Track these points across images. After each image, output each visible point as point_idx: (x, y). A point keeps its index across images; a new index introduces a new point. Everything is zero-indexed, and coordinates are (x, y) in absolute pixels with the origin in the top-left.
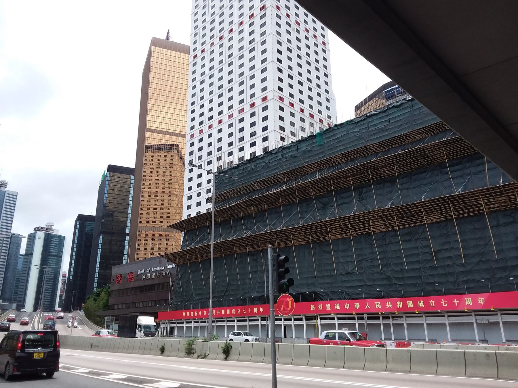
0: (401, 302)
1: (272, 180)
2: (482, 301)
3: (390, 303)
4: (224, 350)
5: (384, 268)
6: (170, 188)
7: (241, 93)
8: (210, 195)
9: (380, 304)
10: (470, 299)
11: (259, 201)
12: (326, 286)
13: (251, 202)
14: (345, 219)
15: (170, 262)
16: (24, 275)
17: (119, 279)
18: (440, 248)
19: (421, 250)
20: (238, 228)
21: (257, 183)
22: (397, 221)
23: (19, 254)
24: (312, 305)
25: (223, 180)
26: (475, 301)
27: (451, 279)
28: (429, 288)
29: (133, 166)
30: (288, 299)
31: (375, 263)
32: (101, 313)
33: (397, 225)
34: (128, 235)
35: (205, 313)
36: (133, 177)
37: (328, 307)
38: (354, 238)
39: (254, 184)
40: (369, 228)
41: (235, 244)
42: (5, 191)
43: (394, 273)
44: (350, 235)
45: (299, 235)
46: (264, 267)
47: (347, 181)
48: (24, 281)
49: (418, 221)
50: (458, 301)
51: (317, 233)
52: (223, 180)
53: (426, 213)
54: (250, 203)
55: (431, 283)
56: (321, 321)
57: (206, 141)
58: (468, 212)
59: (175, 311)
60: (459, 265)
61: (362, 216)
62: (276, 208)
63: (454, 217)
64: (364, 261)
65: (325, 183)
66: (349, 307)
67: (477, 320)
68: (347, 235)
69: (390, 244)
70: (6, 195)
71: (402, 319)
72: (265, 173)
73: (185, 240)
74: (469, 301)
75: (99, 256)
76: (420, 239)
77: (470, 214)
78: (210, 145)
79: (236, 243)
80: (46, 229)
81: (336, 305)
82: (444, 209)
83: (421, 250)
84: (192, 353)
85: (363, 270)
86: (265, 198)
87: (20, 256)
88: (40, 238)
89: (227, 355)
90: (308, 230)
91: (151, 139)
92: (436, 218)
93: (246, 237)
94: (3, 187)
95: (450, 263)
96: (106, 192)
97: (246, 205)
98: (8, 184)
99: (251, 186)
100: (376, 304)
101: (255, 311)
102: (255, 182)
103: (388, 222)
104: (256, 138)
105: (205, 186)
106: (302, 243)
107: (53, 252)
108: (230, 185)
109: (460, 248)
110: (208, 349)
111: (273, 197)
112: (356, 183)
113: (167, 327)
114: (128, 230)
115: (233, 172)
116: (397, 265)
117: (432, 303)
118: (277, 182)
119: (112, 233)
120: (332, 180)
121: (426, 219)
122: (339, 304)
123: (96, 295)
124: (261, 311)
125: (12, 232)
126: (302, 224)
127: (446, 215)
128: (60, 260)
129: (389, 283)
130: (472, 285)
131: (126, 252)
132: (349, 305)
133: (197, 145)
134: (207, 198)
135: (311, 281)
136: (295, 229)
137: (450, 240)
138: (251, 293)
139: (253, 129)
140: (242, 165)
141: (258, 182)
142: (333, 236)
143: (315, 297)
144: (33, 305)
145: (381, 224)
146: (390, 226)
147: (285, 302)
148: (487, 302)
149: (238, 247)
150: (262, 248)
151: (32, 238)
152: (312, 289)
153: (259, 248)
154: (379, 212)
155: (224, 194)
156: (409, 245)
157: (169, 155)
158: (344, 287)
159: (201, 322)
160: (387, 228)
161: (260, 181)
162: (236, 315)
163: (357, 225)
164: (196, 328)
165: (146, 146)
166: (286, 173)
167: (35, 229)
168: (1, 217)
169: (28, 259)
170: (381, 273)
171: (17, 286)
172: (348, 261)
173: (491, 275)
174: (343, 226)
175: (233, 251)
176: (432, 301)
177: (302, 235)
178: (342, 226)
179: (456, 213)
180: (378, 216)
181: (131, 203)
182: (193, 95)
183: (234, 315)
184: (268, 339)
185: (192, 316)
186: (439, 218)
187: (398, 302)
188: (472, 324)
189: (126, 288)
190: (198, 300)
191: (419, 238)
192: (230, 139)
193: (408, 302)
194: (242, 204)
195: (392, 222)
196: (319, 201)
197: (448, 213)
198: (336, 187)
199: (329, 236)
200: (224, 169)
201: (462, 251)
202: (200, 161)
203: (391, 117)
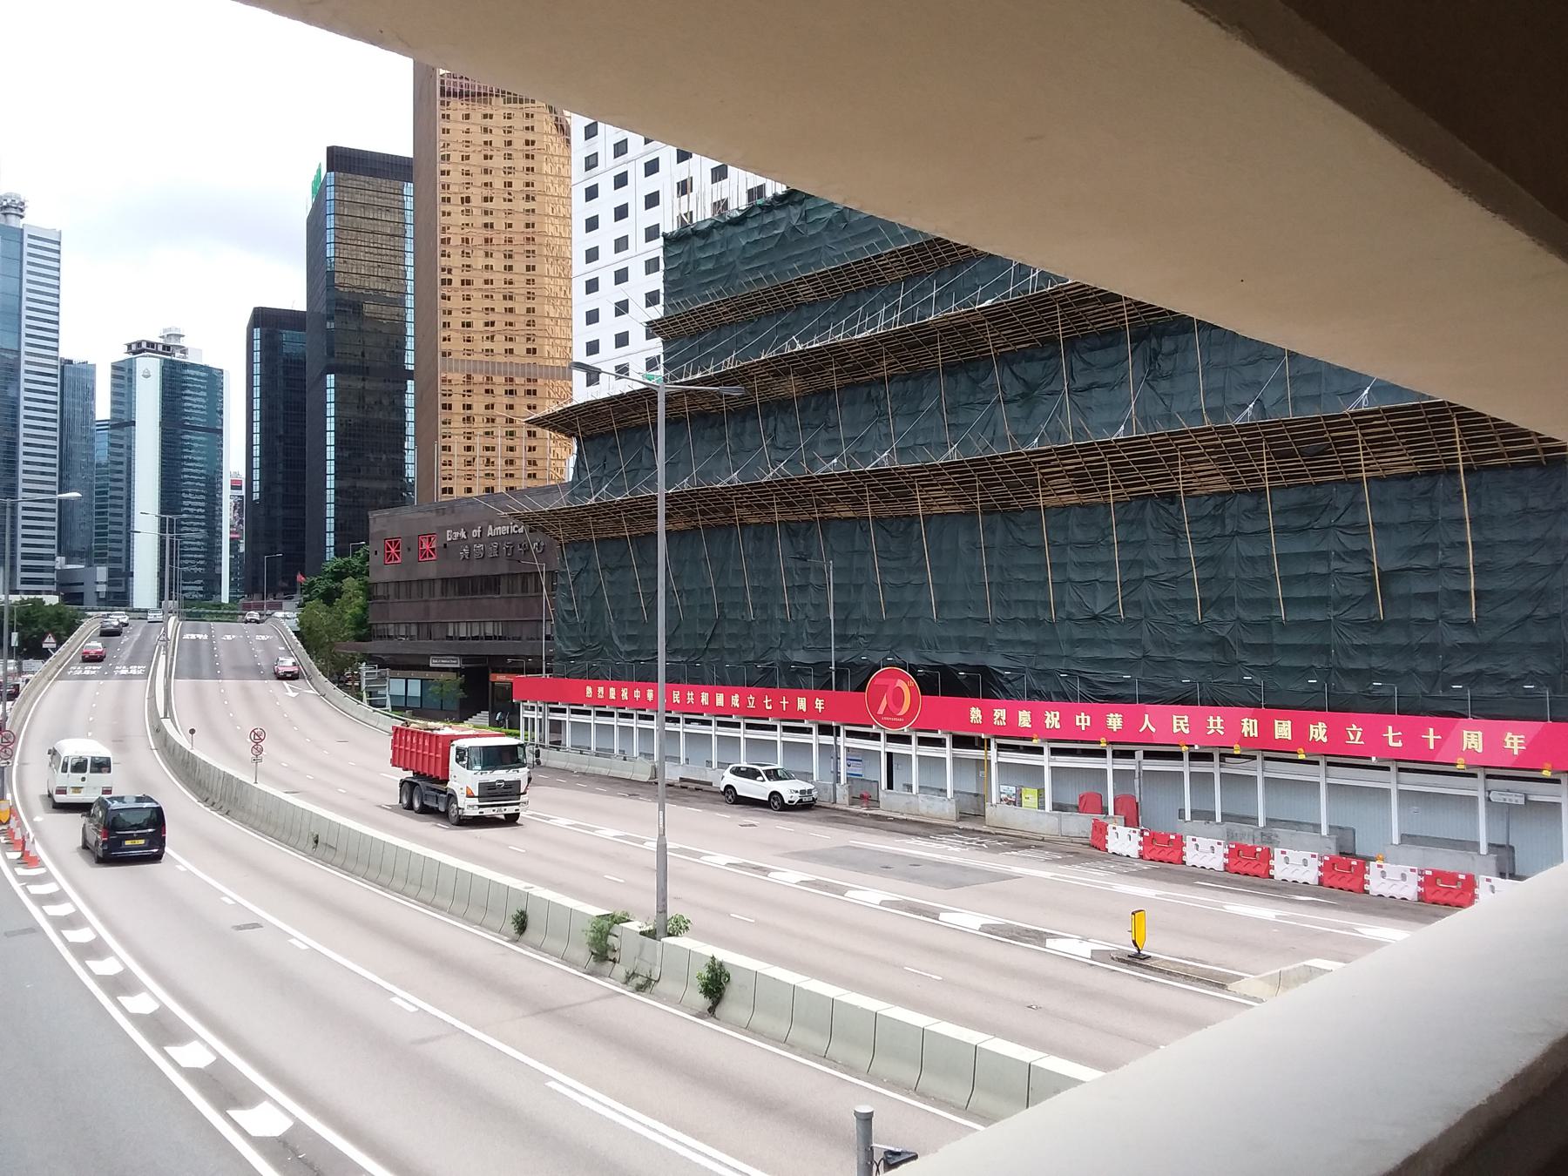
0: (1256, 721)
1: (857, 274)
2: (1516, 744)
3: (1219, 720)
4: (705, 986)
5: (1209, 611)
6: (531, 255)
8: (657, 312)
9: (1186, 721)
10: (1480, 733)
11: (815, 362)
12: (1020, 649)
13: (789, 363)
14: (1096, 449)
16: (119, 468)
17: (393, 550)
18: (1399, 565)
19: (1335, 565)
20: (748, 441)
21: (809, 282)
22: (1267, 464)
23: (94, 421)
24: (973, 708)
25: (697, 262)
26: (1493, 742)
27: (1425, 666)
28: (1351, 688)
29: (403, 146)
30: (901, 683)
31: (1184, 594)
32: (347, 648)
33: (1266, 476)
34: (410, 375)
36: (409, 188)
37: (1024, 719)
38: (1121, 505)
39: (798, 284)
40: (1172, 480)
41: (736, 499)
42: (21, 227)
43: (1241, 629)
44: (1109, 496)
45: (940, 487)
46: (829, 574)
47: (1110, 310)
48: (119, 502)
49: (1339, 468)
50: (1439, 737)
51: (1000, 484)
52: (697, 262)
53: (1370, 447)
54: (784, 364)
55: (1357, 671)
56: (1000, 753)
58: (1511, 454)
59: (562, 679)
60: (1456, 624)
61: (1152, 444)
62: (869, 384)
63: (1461, 463)
64: (1146, 585)
65: (1035, 314)
66: (1088, 724)
67: (1489, 792)
68: (1099, 497)
69: (1238, 534)
70: (27, 241)
72: (833, 244)
73: (581, 466)
74: (1473, 740)
75: (330, 439)
76: (1338, 527)
79: (740, 496)
80: (164, 349)
81: (1048, 714)
82: (1431, 440)
83: (1335, 565)
84: (610, 960)
85: (1141, 610)
86: (834, 353)
87: (98, 426)
88: (148, 377)
89: (715, 999)
90: (973, 476)
92: (1400, 462)
93: (771, 482)
94: (13, 217)
95: (1427, 613)
96: (330, 237)
97: (772, 371)
99: (787, 291)
100: (1175, 721)
101: (799, 707)
102: (801, 279)
103: (1238, 467)
105: (642, 314)
106: (949, 509)
108: (719, 280)
109: (1469, 568)
110: (658, 963)
111: (862, 351)
112: (1140, 318)
113: (540, 720)
115: (730, 235)
116: (1249, 603)
117: (1354, 733)
118: (873, 281)
119: (363, 371)
120: (1061, 307)
121: (1365, 465)
122: (1058, 713)
124: (817, 707)
125: (60, 356)
126: (953, 454)
127: (1438, 457)
129: (1221, 659)
130: (1490, 690)
131: (410, 429)
132: (1088, 718)
133: (609, 199)
134: (647, 323)
135: (971, 633)
136: (930, 471)
137: (1439, 541)
138: (789, 651)
140: (758, 211)
141: (810, 279)
142: (1053, 495)
144: (157, 571)
145: (1214, 472)
146: (1244, 477)
147: (890, 690)
148: (1532, 746)
149: (746, 506)
150: (821, 515)
151: (123, 375)
152: (977, 658)
153: (814, 516)
154: (1213, 434)
155: (703, 311)
156: (1299, 546)
158: (1076, 660)
159: (641, 717)
160: (1231, 484)
161: (818, 274)
162: (743, 711)
163: (1133, 470)
164: (627, 731)
166: (905, 252)
167: (129, 346)
169: (122, 438)
170: (1199, 627)
171: (103, 513)
172: (1097, 580)
173: (1557, 664)
174: (1087, 471)
175: (731, 517)
176: (1354, 728)
177: (951, 486)
178: (1083, 468)
179: (1470, 453)
180: (1205, 447)
183: (737, 711)
184: (837, 786)
185: (614, 698)
186: (1411, 465)
187: (1245, 720)
190: (629, 654)
191: (1337, 524)
193: (1276, 722)
194: (757, 367)
195: (1253, 466)
198: (1072, 328)
199: (1038, 496)
200: (698, 223)
201: (1468, 524)
202: (621, 159)
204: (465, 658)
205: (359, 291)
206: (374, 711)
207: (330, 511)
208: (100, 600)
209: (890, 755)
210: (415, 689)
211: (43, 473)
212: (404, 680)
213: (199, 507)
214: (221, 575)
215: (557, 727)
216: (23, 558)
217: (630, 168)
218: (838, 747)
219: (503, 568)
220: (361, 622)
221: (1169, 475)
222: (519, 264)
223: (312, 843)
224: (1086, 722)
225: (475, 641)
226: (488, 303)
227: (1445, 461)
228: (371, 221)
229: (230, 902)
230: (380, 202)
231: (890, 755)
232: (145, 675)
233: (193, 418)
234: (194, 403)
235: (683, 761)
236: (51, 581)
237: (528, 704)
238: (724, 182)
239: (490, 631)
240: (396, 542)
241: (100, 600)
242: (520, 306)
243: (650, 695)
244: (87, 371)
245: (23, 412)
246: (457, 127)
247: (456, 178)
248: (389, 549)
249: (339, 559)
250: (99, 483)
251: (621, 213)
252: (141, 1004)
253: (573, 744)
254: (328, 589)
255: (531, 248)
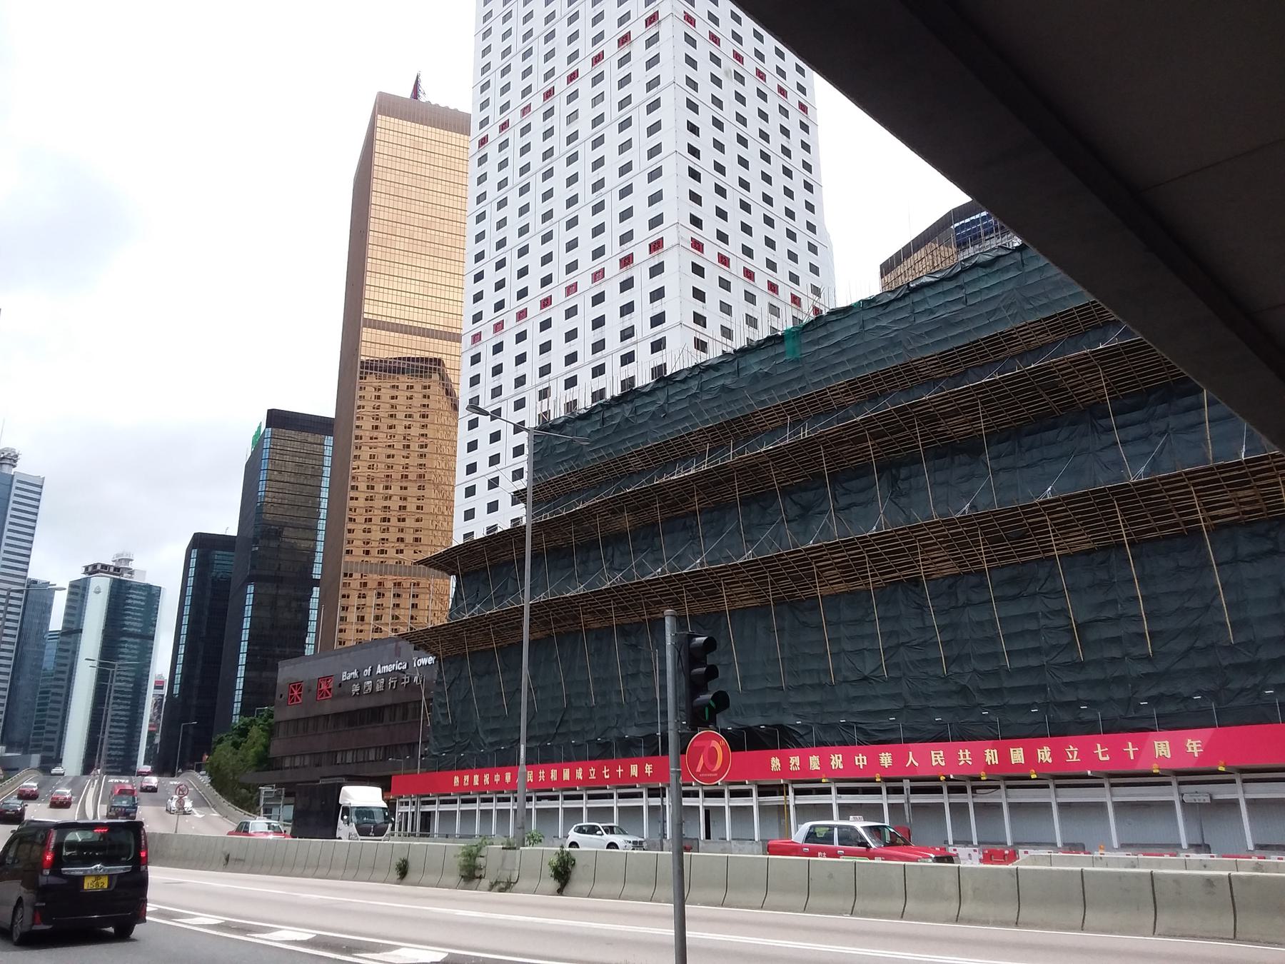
0: (995, 751)
1: (675, 448)
2: (1195, 748)
3: (967, 753)
4: (555, 869)
5: (952, 666)
6: (423, 467)
7: (598, 231)
8: (521, 484)
9: (942, 755)
10: (1167, 742)
11: (643, 500)
12: (808, 709)
13: (623, 502)
14: (856, 543)
15: (422, 652)
16: (60, 683)
17: (296, 693)
18: (1092, 616)
19: (1043, 622)
20: (591, 566)
21: (638, 455)
22: (984, 549)
23: (47, 631)
24: (773, 758)
25: (554, 447)
26: (1178, 748)
27: (1119, 693)
28: (1065, 716)
30: (715, 744)
31: (931, 654)
32: (250, 777)
33: (984, 559)
34: (317, 583)
36: (329, 440)
37: (814, 763)
38: (878, 590)
39: (630, 457)
40: (915, 567)
41: (582, 606)
42: (12, 474)
43: (977, 678)
44: (869, 583)
45: (741, 584)
46: (655, 663)
47: (860, 449)
48: (59, 698)
49: (1037, 548)
50: (1137, 749)
51: (786, 578)
52: (554, 447)
53: (1057, 529)
54: (620, 503)
56: (797, 796)
57: (512, 350)
58: (1162, 528)
59: (434, 773)
60: (1139, 659)
61: (897, 537)
62: (686, 516)
63: (1125, 539)
65: (805, 454)
66: (865, 763)
67: (1182, 795)
68: (862, 585)
69: (969, 605)
70: (15, 484)
71: (997, 792)
72: (656, 429)
73: (459, 596)
74: (1162, 748)
75: (245, 635)
76: (1042, 593)
77: (1166, 532)
78: (521, 359)
79: (585, 603)
80: (115, 570)
81: (833, 757)
82: (1101, 520)
83: (1043, 622)
84: (477, 878)
85: (900, 670)
86: (658, 492)
87: (50, 635)
88: (99, 592)
89: (563, 881)
90: (765, 573)
91: (375, 346)
92: (1081, 541)
93: (610, 589)
94: (8, 466)
95: (1115, 652)
96: (263, 476)
97: (610, 510)
98: (19, 456)
99: (622, 463)
100: (933, 755)
101: (632, 774)
102: (632, 453)
103: (963, 553)
104: (636, 343)
106: (749, 603)
107: (132, 626)
108: (571, 459)
109: (1142, 616)
110: (517, 868)
111: (678, 489)
112: (882, 455)
113: (413, 813)
114: (317, 571)
115: (579, 426)
116: (984, 657)
117: (1072, 752)
118: (686, 453)
119: (277, 580)
120: (824, 448)
121: (1056, 545)
122: (840, 756)
123: (238, 734)
124: (646, 772)
125: (29, 576)
126: (748, 555)
127: (1107, 534)
129: (964, 703)
130: (1171, 708)
131: (312, 627)
132: (865, 758)
134: (514, 493)
135: (770, 699)
136: (732, 570)
137: (1117, 597)
138: (623, 728)
139: (627, 321)
140: (600, 409)
141: (639, 453)
142: (826, 585)
143: (781, 738)
144: (82, 758)
145: (946, 558)
146: (968, 561)
147: (706, 751)
148: (1208, 749)
149: (590, 612)
150: (649, 617)
151: (78, 592)
152: (775, 718)
153: (643, 617)
154: (941, 526)
155: (557, 482)
156: (1014, 610)
157: (418, 384)
158: (853, 714)
159: (499, 800)
160: (959, 567)
161: (645, 449)
162: (586, 783)
163: (885, 560)
164: (486, 814)
165: (362, 362)
166: (710, 430)
167: (87, 568)
169: (68, 643)
170: (945, 679)
171: (43, 710)
173: (1218, 683)
174: (851, 563)
175: (577, 624)
176: (1072, 748)
177: (749, 583)
178: (847, 561)
179: (1132, 529)
180: (937, 537)
181: (324, 504)
182: (480, 237)
183: (580, 782)
184: (664, 841)
185: (478, 784)
186: (1089, 542)
187: (987, 751)
188: (1171, 804)
189: (312, 714)
190: (492, 744)
191: (1040, 591)
192: (570, 346)
193: (1011, 750)
194: (599, 506)
195: (973, 551)
197: (1111, 529)
198: (833, 465)
199: (815, 587)
200: (555, 420)
201: (1145, 623)
202: (496, 399)
203: (970, 291)
215: (427, 817)
221: (912, 562)
224: (859, 759)
240: (299, 686)
243: (508, 777)
246: (370, 393)
247: (363, 465)
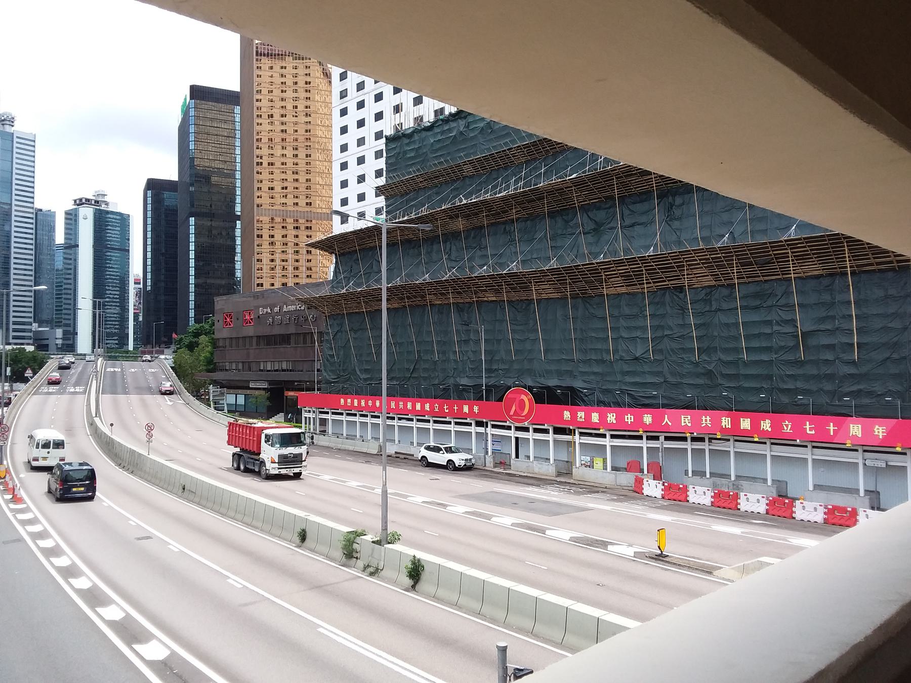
0: (729, 419)
1: (498, 159)
2: (881, 432)
3: (708, 418)
4: (410, 573)
5: (703, 355)
6: (308, 148)
8: (382, 181)
9: (689, 419)
10: (860, 426)
11: (473, 210)
12: (593, 377)
13: (458, 211)
14: (637, 261)
16: (69, 272)
17: (228, 320)
18: (813, 328)
19: (776, 328)
20: (435, 256)
21: (470, 164)
22: (736, 270)
23: (54, 245)
24: (565, 411)
25: (405, 152)
26: (867, 431)
27: (828, 387)
28: (785, 400)
29: (234, 85)
30: (523, 397)
31: (688, 345)
32: (202, 377)
33: (736, 277)
34: (238, 218)
35: (378, 404)
36: (237, 109)
37: (595, 417)
38: (651, 294)
39: (464, 165)
40: (681, 279)
41: (428, 290)
42: (12, 132)
43: (721, 365)
44: (644, 288)
45: (546, 283)
46: (482, 334)
47: (645, 180)
48: (69, 292)
49: (778, 272)
50: (836, 428)
51: (581, 281)
52: (405, 152)
53: (796, 259)
54: (456, 212)
56: (581, 437)
58: (878, 264)
59: (327, 394)
60: (846, 363)
61: (669, 258)
62: (505, 223)
63: (849, 269)
65: (601, 182)
66: (632, 420)
67: (865, 460)
68: (639, 289)
69: (719, 310)
70: (15, 140)
72: (484, 142)
73: (338, 271)
74: (856, 430)
75: (192, 255)
76: (777, 306)
79: (430, 288)
80: (95, 202)
81: (609, 415)
82: (831, 255)
83: (776, 328)
84: (355, 558)
85: (663, 354)
86: (485, 205)
87: (57, 247)
88: (86, 219)
89: (415, 580)
90: (565, 277)
92: (814, 268)
93: (448, 280)
94: (8, 126)
95: (829, 356)
96: (192, 138)
97: (448, 215)
99: (457, 169)
100: (683, 419)
101: (464, 411)
102: (465, 162)
103: (719, 271)
106: (551, 296)
108: (418, 163)
109: (854, 330)
110: (382, 559)
111: (501, 204)
112: (662, 185)
113: (314, 418)
115: (424, 136)
116: (726, 351)
117: (787, 426)
118: (507, 163)
119: (211, 216)
120: (616, 178)
121: (793, 270)
122: (614, 414)
124: (474, 411)
125: (35, 207)
126: (553, 264)
127: (835, 265)
128: (126, 317)
129: (709, 382)
130: (866, 401)
131: (238, 249)
132: (632, 417)
134: (376, 187)
135: (564, 367)
136: (540, 273)
137: (836, 314)
138: (458, 378)
140: (441, 123)
141: (471, 162)
142: (612, 288)
144: (91, 331)
145: (705, 274)
146: (723, 277)
147: (517, 401)
148: (890, 433)
149: (434, 294)
150: (477, 299)
151: (72, 218)
152: (568, 382)
153: (473, 299)
154: (705, 252)
155: (408, 181)
156: (755, 317)
158: (625, 384)
159: (373, 417)
160: (715, 281)
161: (475, 159)
162: (432, 413)
163: (658, 273)
164: (364, 425)
166: (526, 146)
167: (75, 201)
168: (11, 308)
169: (71, 254)
170: (697, 364)
171: (60, 298)
173: (905, 386)
174: (631, 273)
175: (425, 300)
176: (787, 423)
177: (553, 282)
178: (629, 272)
179: (854, 263)
180: (700, 260)
183: (428, 413)
184: (487, 457)
185: (357, 405)
186: (820, 270)
187: (723, 418)
190: (365, 380)
191: (777, 304)
193: (742, 419)
194: (440, 213)
195: (728, 270)
196: (587, 214)
198: (623, 191)
199: (603, 288)
200: (405, 129)
201: (853, 304)
202: (361, 92)
204: (270, 382)
205: (209, 169)
206: (217, 413)
207: (192, 297)
208: (58, 348)
209: (517, 439)
210: (241, 400)
211: (25, 275)
212: (235, 395)
213: (116, 295)
214: (128, 334)
216: (13, 324)
217: (366, 98)
218: (487, 434)
219: (292, 330)
220: (209, 361)
222: (302, 153)
223: (181, 490)
224: (631, 419)
225: (276, 373)
226: (283, 176)
227: (840, 268)
228: (216, 129)
229: (134, 524)
230: (221, 117)
231: (517, 439)
232: (85, 392)
233: (112, 243)
234: (113, 234)
235: (397, 442)
236: (29, 338)
237: (307, 409)
238: (421, 106)
239: (284, 367)
240: (230, 315)
241: (58, 348)
242: (302, 178)
244: (51, 215)
245: (13, 239)
246: (265, 74)
248: (226, 319)
249: (197, 325)
250: (58, 280)
251: (361, 123)
252: (82, 583)
253: (333, 432)
254: (191, 342)
255: (308, 144)
